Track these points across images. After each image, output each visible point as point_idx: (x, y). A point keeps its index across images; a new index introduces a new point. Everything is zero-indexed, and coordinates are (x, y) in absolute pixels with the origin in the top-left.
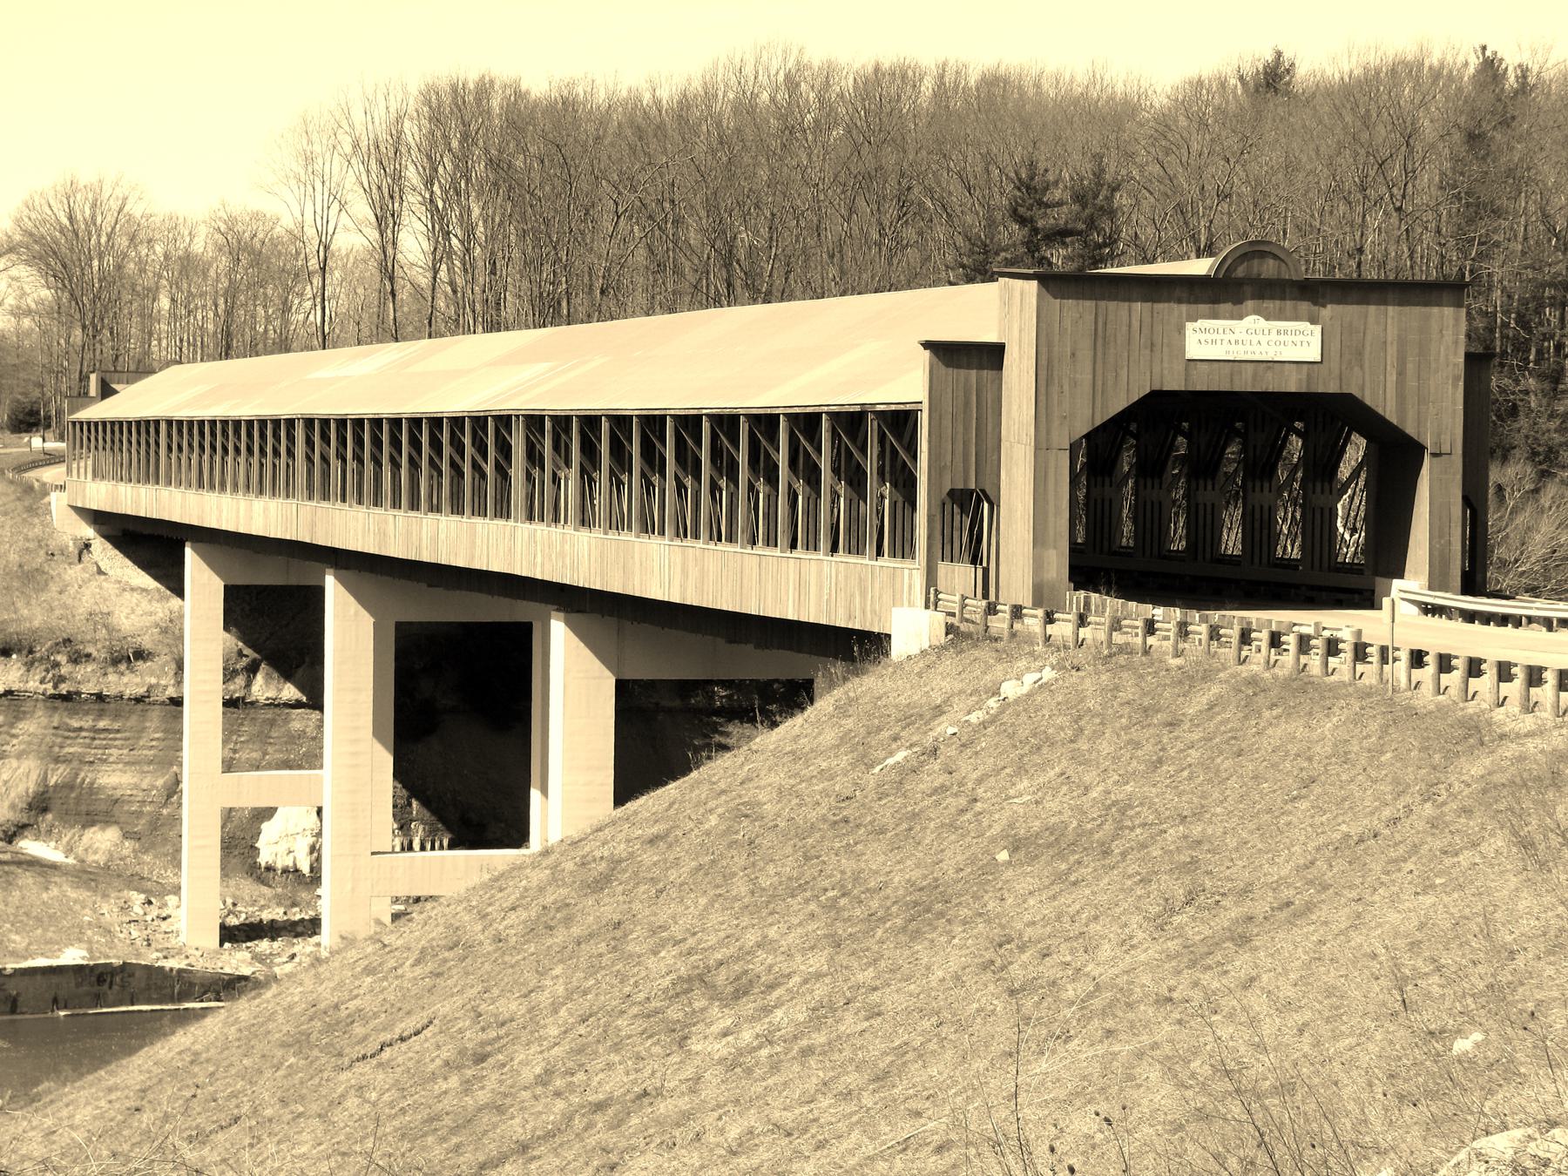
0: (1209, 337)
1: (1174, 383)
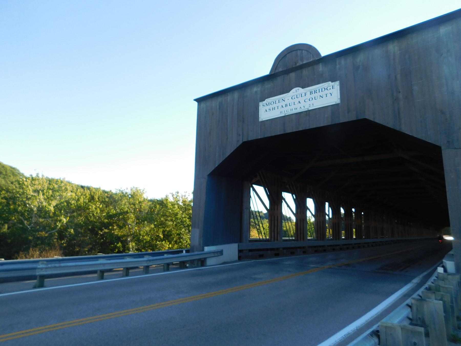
0: (271, 107)
1: (252, 136)
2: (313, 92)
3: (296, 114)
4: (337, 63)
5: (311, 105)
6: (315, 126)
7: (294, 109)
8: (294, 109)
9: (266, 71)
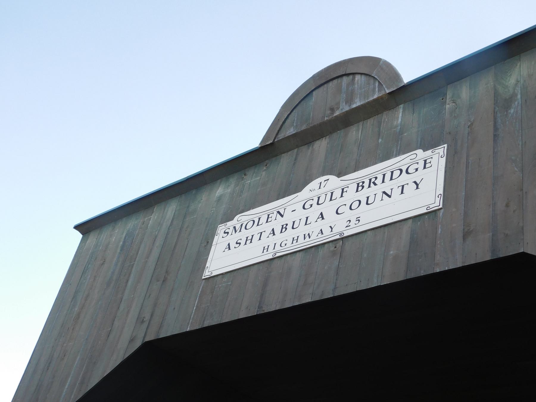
0: (243, 235)
4: (449, 95)
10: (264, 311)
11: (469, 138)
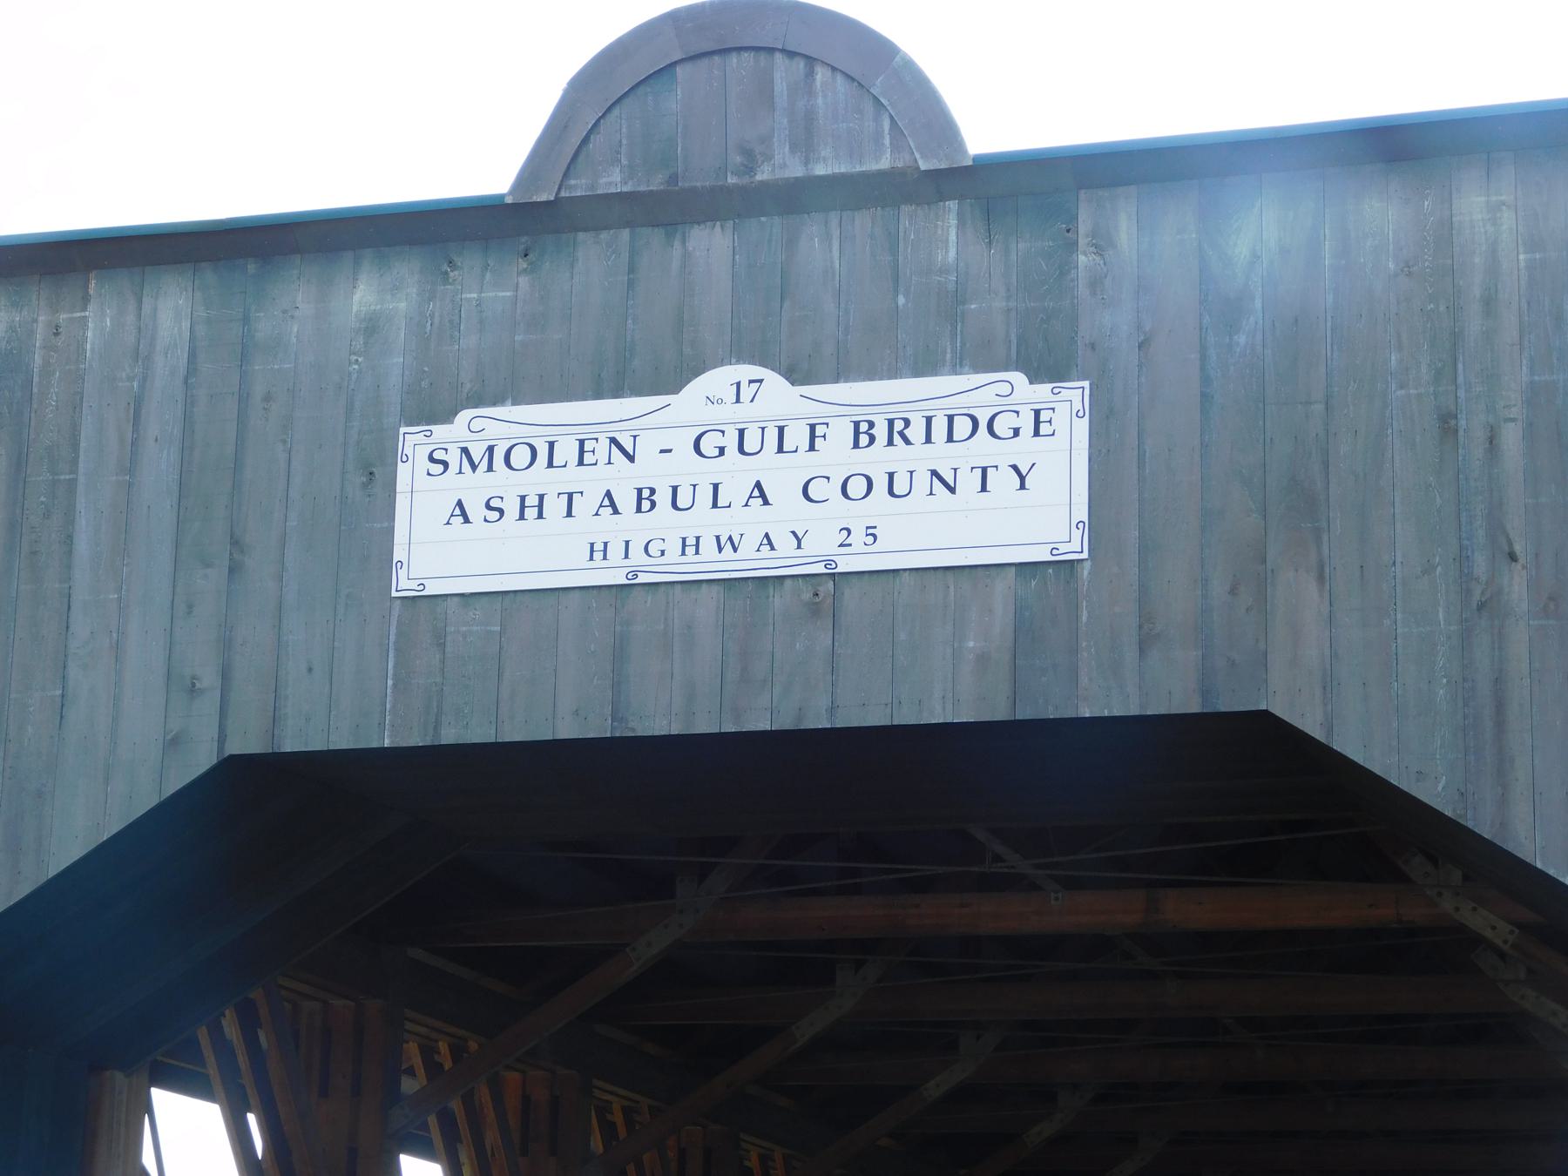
0: (506, 484)
1: (320, 722)
2: (881, 431)
3: (729, 584)
5: (858, 538)
6: (875, 717)
7: (708, 546)
8: (708, 546)
9: (480, 153)
10: (633, 730)
11: (1143, 380)
